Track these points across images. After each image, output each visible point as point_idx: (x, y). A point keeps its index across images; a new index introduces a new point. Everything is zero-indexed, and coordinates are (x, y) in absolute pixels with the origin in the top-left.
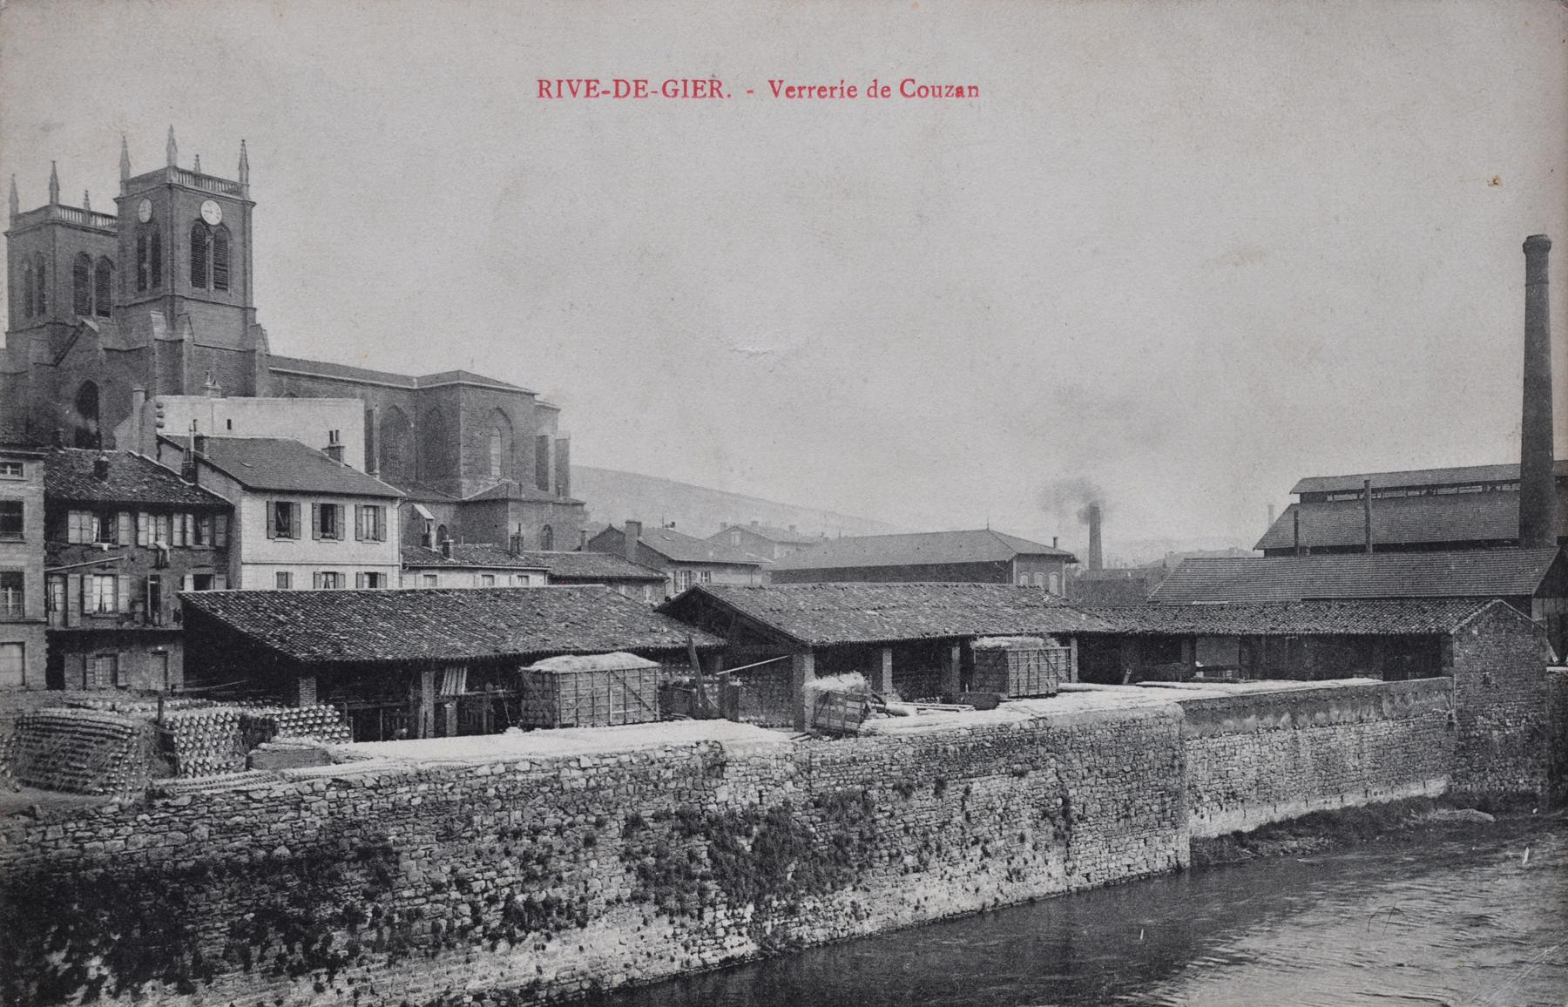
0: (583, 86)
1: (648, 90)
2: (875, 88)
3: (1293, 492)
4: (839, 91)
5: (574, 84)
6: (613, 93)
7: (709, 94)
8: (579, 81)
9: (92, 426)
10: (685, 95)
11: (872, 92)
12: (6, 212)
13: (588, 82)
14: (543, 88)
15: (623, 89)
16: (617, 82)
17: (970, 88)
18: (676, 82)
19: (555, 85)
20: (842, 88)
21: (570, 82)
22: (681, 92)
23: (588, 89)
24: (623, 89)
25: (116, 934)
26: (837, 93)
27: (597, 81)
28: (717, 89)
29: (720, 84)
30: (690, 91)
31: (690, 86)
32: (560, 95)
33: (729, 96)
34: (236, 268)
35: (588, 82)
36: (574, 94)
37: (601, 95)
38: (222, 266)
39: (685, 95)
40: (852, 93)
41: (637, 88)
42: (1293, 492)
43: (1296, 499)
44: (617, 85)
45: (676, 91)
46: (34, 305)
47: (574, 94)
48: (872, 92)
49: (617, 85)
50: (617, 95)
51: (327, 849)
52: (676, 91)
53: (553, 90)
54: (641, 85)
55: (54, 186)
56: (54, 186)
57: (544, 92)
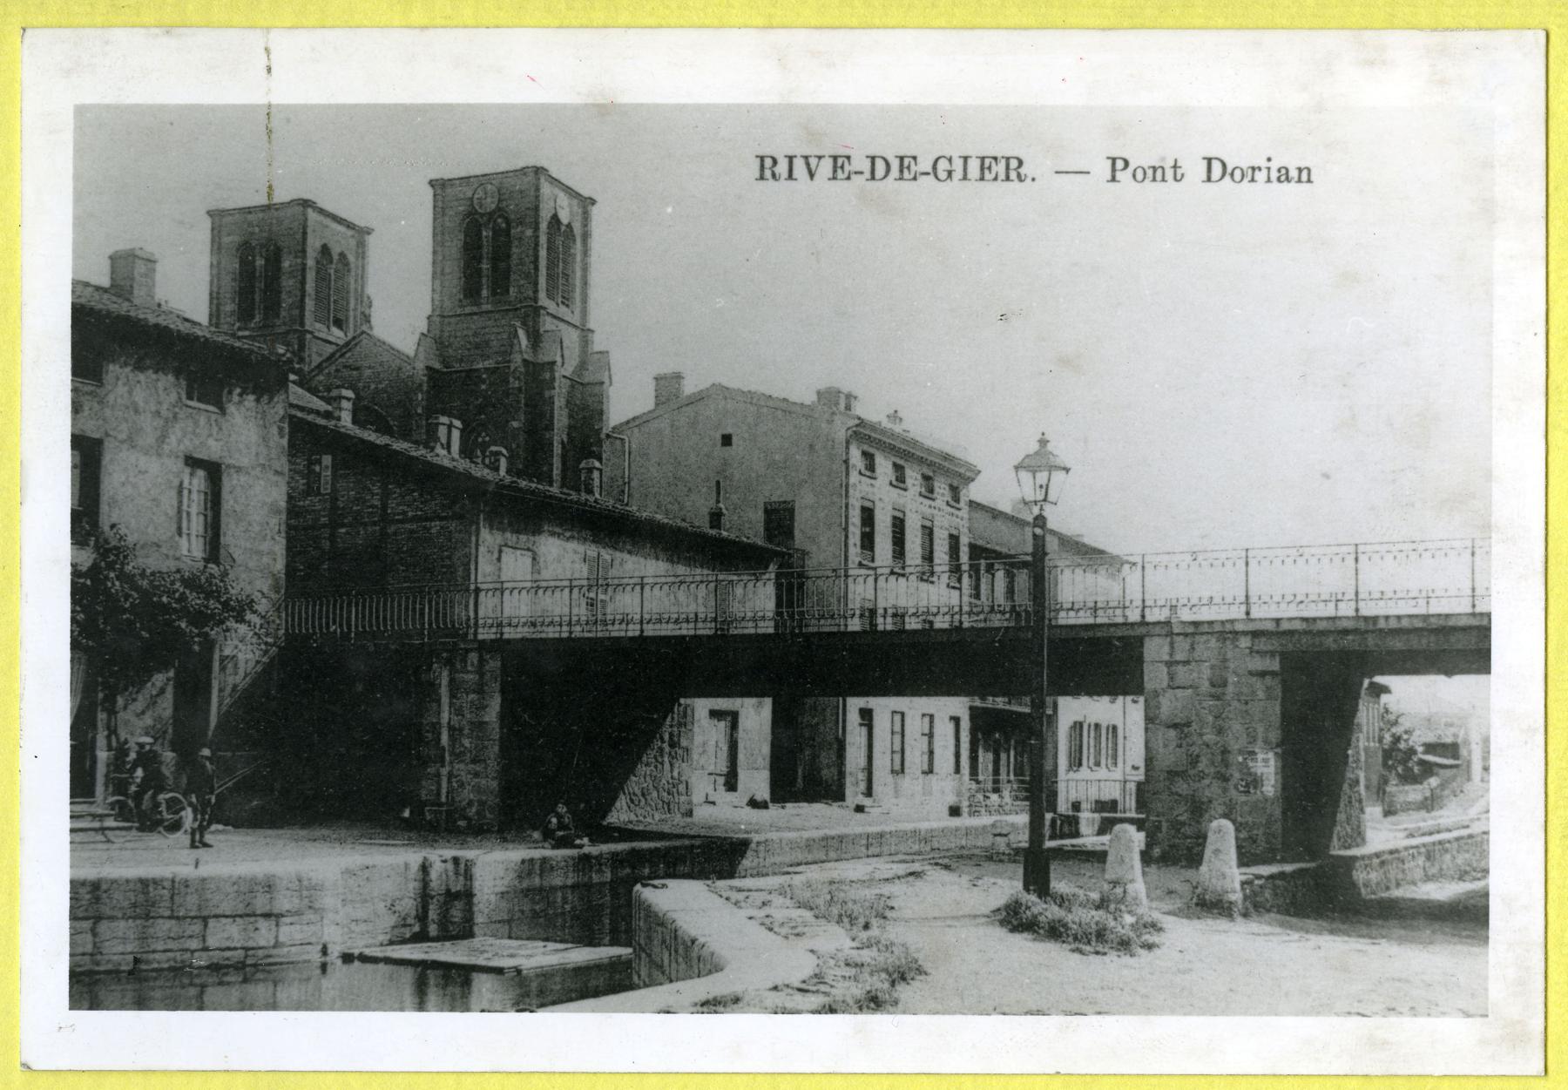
4: (1265, 172)
5: (813, 162)
6: (867, 175)
7: (1002, 176)
9: (858, 612)
10: (965, 178)
13: (835, 158)
14: (1117, 165)
15: (880, 167)
16: (873, 159)
17: (1300, 170)
20: (1269, 169)
22: (958, 174)
23: (982, 168)
24: (880, 167)
25: (550, 822)
26: (1261, 176)
29: (1021, 163)
32: (790, 176)
33: (1033, 179)
34: (455, 245)
35: (835, 158)
37: (853, 176)
38: (472, 250)
39: (965, 178)
44: (873, 164)
45: (950, 173)
46: (485, 266)
47: (812, 175)
49: (873, 164)
50: (873, 178)
52: (950, 173)
53: (782, 168)
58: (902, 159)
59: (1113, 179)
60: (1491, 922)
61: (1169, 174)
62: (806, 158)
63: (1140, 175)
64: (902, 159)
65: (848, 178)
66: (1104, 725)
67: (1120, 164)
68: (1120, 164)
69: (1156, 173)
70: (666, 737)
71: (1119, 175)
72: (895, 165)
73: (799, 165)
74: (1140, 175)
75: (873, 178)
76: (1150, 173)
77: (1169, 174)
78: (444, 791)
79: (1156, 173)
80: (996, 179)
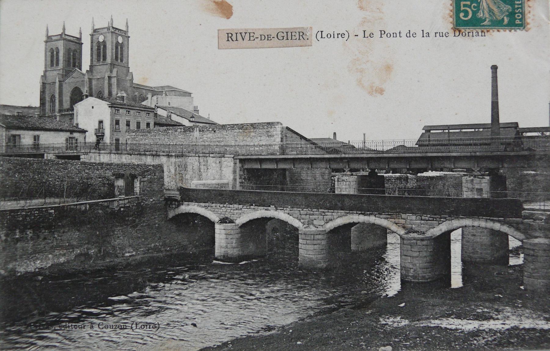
0: (248, 35)
1: (271, 37)
2: (410, 33)
3: (423, 129)
4: (471, 33)
5: (243, 34)
7: (298, 38)
8: (246, 33)
11: (408, 35)
12: (45, 33)
14: (381, 37)
18: (283, 33)
19: (234, 35)
21: (241, 33)
22: (285, 38)
24: (329, 36)
27: (254, 33)
28: (231, 37)
30: (290, 37)
31: (289, 34)
36: (243, 39)
39: (287, 39)
40: (343, 36)
41: (268, 37)
42: (423, 129)
43: (424, 131)
48: (408, 35)
51: (6, 181)
53: (234, 38)
54: (269, 36)
55: (64, 29)
56: (64, 29)
57: (230, 39)
58: (268, 35)
59: (381, 37)
60: (491, 103)
61: (398, 35)
62: (241, 33)
63: (389, 35)
64: (268, 35)
65: (254, 40)
66: (54, 48)
67: (383, 32)
68: (383, 32)
69: (395, 35)
70: (411, 266)
71: (382, 36)
72: (267, 37)
73: (239, 36)
74: (389, 35)
75: (261, 40)
76: (392, 35)
77: (398, 35)
78: (63, 319)
79: (395, 35)
80: (296, 39)
